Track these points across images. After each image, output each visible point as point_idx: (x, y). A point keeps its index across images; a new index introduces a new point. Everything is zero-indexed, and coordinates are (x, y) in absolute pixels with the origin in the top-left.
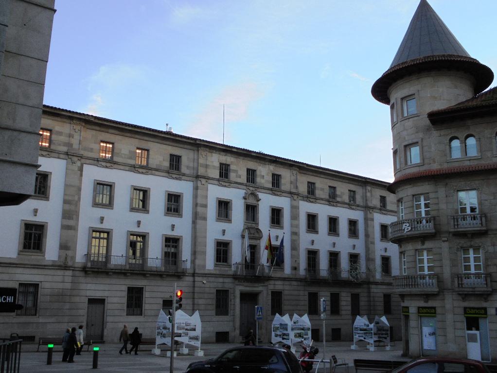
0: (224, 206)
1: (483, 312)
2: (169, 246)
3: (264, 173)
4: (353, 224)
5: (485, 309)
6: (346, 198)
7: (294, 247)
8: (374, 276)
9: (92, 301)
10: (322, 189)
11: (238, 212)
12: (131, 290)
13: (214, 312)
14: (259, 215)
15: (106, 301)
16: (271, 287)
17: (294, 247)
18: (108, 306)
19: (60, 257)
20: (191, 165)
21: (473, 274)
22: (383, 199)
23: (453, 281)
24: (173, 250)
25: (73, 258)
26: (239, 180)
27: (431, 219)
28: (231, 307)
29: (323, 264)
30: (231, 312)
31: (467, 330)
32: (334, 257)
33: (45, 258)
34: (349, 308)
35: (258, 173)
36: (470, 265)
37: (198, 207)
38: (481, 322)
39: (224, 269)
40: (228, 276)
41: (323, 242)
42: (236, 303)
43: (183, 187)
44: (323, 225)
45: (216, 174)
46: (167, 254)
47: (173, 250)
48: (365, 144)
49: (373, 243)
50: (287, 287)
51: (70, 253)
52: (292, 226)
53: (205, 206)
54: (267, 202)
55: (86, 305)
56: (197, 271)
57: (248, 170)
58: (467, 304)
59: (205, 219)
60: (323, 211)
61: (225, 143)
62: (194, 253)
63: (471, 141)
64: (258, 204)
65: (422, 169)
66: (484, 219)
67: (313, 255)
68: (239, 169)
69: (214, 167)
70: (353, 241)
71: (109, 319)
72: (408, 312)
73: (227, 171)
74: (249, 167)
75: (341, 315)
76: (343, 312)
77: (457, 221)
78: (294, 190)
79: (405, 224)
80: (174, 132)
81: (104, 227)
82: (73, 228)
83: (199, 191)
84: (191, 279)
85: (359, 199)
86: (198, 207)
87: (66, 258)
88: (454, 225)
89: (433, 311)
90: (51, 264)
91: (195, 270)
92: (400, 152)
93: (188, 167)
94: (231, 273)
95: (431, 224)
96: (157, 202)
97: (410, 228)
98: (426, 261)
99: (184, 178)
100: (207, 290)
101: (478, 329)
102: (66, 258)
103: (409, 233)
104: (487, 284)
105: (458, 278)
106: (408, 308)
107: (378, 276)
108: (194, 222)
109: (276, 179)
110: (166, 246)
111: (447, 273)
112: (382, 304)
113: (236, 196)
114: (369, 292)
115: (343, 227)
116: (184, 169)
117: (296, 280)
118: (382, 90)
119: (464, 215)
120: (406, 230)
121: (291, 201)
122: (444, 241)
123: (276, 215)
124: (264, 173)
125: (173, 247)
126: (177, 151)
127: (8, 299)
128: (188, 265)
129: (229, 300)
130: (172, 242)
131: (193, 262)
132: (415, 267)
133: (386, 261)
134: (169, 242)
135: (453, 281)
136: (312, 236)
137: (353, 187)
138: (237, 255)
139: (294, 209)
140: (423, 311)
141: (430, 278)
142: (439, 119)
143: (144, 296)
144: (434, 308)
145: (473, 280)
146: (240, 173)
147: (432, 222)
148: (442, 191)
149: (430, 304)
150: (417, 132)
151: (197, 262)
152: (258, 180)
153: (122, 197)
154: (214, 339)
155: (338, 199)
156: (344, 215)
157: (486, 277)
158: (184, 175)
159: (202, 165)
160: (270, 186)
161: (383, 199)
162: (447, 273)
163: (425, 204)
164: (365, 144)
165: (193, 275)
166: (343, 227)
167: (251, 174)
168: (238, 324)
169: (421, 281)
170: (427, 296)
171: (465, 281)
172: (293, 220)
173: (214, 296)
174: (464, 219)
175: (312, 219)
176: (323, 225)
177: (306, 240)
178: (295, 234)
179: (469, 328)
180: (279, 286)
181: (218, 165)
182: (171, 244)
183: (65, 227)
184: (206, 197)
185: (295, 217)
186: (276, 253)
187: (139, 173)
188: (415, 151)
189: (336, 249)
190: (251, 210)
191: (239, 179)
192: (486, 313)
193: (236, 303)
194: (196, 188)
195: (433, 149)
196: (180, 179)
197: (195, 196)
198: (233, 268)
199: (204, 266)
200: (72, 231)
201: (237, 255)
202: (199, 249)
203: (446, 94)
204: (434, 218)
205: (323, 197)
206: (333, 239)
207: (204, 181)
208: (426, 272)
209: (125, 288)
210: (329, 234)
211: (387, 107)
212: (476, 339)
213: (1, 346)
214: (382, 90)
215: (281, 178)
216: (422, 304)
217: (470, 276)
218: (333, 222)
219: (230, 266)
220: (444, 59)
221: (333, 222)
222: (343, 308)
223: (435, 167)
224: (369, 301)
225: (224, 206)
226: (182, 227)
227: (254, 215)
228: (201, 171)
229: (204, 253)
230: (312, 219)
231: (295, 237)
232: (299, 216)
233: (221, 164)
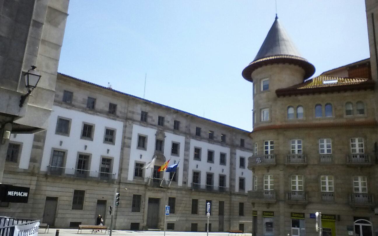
0: (142, 141)
1: (302, 216)
2: (104, 164)
3: (169, 120)
4: (223, 156)
5: (304, 214)
6: (220, 139)
7: (186, 169)
8: (234, 190)
9: (49, 199)
10: (205, 132)
11: (151, 144)
12: (76, 192)
13: (131, 210)
14: (165, 147)
15: (59, 199)
16: (169, 195)
17: (186, 169)
18: (60, 202)
19: (29, 167)
20: (123, 111)
21: (297, 192)
22: (242, 141)
23: (285, 196)
24: (107, 166)
25: (39, 168)
26: (153, 123)
27: (275, 155)
28: (142, 206)
29: (203, 182)
30: (142, 210)
31: (293, 227)
32: (210, 177)
33: (19, 167)
34: (218, 210)
35: (166, 119)
36: (326, 187)
37: (126, 138)
38: (301, 223)
39: (139, 180)
40: (142, 185)
41: (203, 167)
42: (145, 205)
43: (117, 125)
44: (204, 155)
45: (139, 118)
46: (102, 169)
47: (107, 166)
48: (235, 107)
49: (235, 169)
50: (179, 195)
51: (37, 165)
52: (185, 155)
53: (130, 139)
54: (170, 138)
55: (44, 201)
56: (122, 181)
57: (159, 118)
58: (292, 210)
59: (129, 147)
60: (205, 147)
61: (145, 99)
62: (121, 169)
63: (300, 110)
64: (164, 140)
65: (270, 124)
66: (305, 158)
67: (196, 175)
68: (154, 116)
69: (138, 114)
70: (223, 167)
71: (60, 211)
72: (257, 214)
73: (146, 116)
74: (160, 115)
75: (199, 214)
76: (200, 213)
77: (290, 158)
78: (187, 132)
79: (257, 159)
80: (113, 88)
81: (62, 148)
82: (41, 148)
83: (127, 128)
84: (117, 186)
85: (227, 139)
86: (126, 138)
87: (34, 168)
88: (288, 161)
89: (272, 214)
90: (23, 171)
91: (120, 180)
92: (257, 111)
93: (121, 112)
94: (144, 183)
95: (274, 159)
96: (99, 134)
97: (261, 161)
98: (269, 182)
99: (118, 119)
100: (127, 194)
101: (298, 227)
102: (34, 168)
103: (260, 164)
104: (305, 198)
105: (289, 194)
106: (256, 211)
107: (237, 189)
108: (122, 149)
109: (177, 125)
110: (102, 164)
111: (282, 189)
112: (238, 208)
113: (151, 133)
114: (231, 201)
115: (217, 158)
116: (118, 113)
117: (185, 190)
118: (248, 73)
119: (294, 155)
120: (258, 162)
121: (186, 138)
122: (281, 170)
123: (175, 148)
124: (169, 120)
125: (107, 164)
126: (114, 102)
127: (24, 194)
128: (116, 177)
129: (141, 201)
130: (107, 162)
131: (119, 175)
132: (262, 186)
133: (242, 181)
134: (105, 161)
135: (285, 196)
136: (197, 162)
137: (224, 132)
138: (148, 172)
139: (187, 144)
140: (325, 217)
141: (271, 193)
142: (281, 93)
143: (85, 197)
144: (273, 212)
145: (296, 196)
146: (154, 118)
147: (274, 157)
148: (281, 139)
149: (271, 209)
150: (269, 101)
151: (123, 175)
152: (166, 124)
153: (76, 129)
154: (130, 228)
155: (215, 139)
156: (218, 149)
157: (305, 194)
158: (118, 117)
159: (130, 112)
160: (173, 128)
161: (242, 141)
162: (282, 189)
163: (327, 150)
164: (235, 107)
165: (119, 183)
166: (217, 158)
167: (161, 120)
168: (146, 218)
169: (266, 195)
170: (269, 205)
171: (292, 196)
172: (186, 151)
173: (132, 198)
174: (294, 157)
175: (198, 151)
176: (204, 155)
177: (193, 164)
178: (186, 160)
179: (293, 226)
180: (174, 194)
181: (140, 112)
182: (106, 162)
183: (35, 147)
184: (131, 133)
185: (187, 149)
186: (173, 171)
187: (89, 113)
188: (266, 111)
189: (212, 171)
190: (159, 144)
191: (168, 124)
192: (304, 217)
193: (145, 205)
194: (125, 126)
195: (277, 112)
196: (115, 120)
197: (124, 132)
198: (145, 181)
199: (127, 178)
200: (40, 150)
201: (148, 172)
202: (124, 167)
203: (287, 79)
204: (276, 155)
205: (205, 137)
206: (210, 164)
207: (130, 122)
208: (269, 189)
209: (72, 191)
210: (220, 164)
211: (251, 84)
212: (298, 232)
213: (1, 229)
214: (248, 73)
215: (180, 123)
216: (265, 209)
217: (296, 193)
218: (211, 155)
219: (143, 179)
220: (284, 57)
221: (211, 155)
222: (200, 210)
223: (278, 123)
224: (230, 207)
225: (142, 141)
226: (114, 151)
227: (144, 144)
228: (130, 115)
229: (127, 170)
230: (198, 151)
231: (186, 163)
232: (189, 149)
233: (142, 112)
